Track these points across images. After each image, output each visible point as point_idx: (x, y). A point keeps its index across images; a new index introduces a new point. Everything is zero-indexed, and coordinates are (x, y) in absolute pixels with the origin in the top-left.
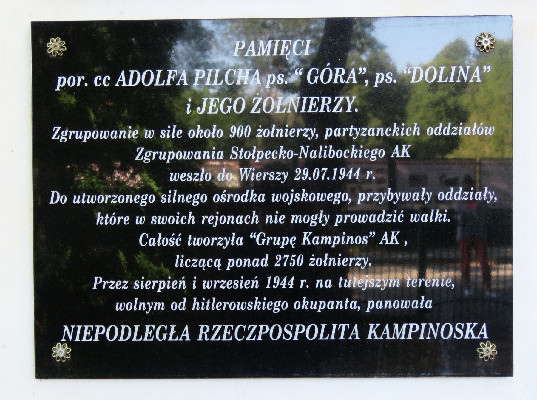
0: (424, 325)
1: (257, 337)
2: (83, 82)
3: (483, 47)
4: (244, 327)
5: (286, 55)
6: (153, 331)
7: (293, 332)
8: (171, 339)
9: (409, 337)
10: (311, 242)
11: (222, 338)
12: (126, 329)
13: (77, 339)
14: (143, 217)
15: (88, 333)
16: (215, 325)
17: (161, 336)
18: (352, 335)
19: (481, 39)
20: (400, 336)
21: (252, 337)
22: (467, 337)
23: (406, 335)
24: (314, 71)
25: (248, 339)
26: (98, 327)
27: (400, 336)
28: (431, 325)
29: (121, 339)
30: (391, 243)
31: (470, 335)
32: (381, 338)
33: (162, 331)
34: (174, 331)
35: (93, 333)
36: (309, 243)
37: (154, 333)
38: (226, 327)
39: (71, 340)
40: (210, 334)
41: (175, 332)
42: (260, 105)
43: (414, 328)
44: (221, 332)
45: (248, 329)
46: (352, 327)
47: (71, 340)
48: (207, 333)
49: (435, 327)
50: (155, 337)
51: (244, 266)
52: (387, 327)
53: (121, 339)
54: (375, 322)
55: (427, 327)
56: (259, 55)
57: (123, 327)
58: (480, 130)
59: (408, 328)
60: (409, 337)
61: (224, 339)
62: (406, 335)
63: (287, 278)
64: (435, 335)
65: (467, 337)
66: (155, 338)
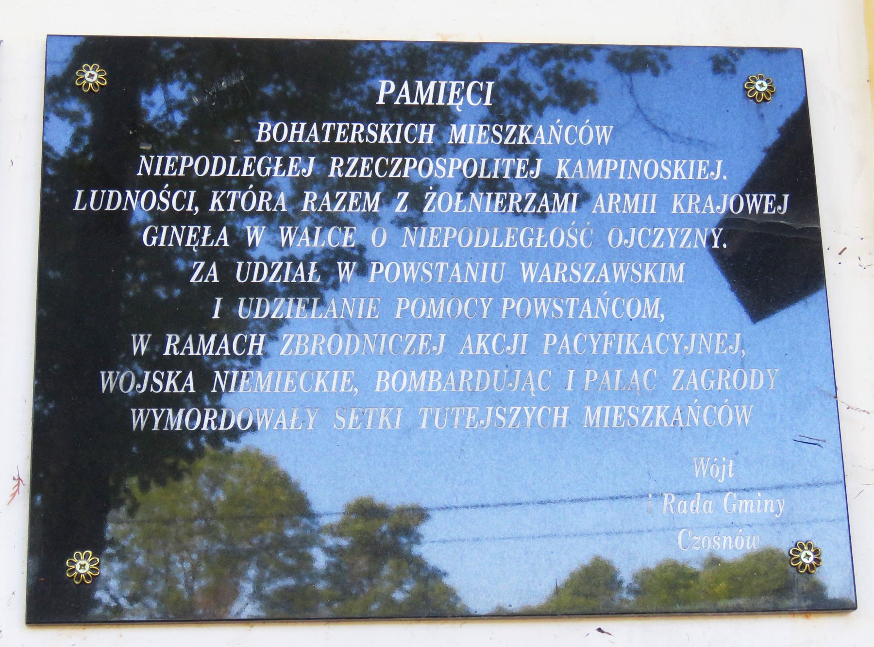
0: (623, 162)
3: (803, 565)
4: (387, 160)
5: (194, 246)
6: (253, 163)
7: (447, 167)
8: (538, 245)
9: (607, 177)
11: (359, 173)
12: (220, 161)
13: (157, 173)
17: (526, 241)
19: (802, 547)
20: (426, 100)
21: (396, 174)
22: (167, 390)
23: (603, 173)
25: (391, 175)
26: (184, 158)
27: (426, 100)
29: (213, 174)
31: (172, 387)
32: (182, 354)
33: (527, 235)
34: (280, 164)
35: (178, 165)
37: (255, 166)
38: (365, 160)
39: (149, 174)
40: (345, 168)
41: (282, 165)
43: (612, 164)
44: (358, 167)
45: (392, 163)
47: (149, 174)
48: (340, 167)
49: (637, 164)
50: (256, 172)
53: (213, 174)
55: (628, 164)
57: (216, 158)
59: (605, 163)
60: (607, 177)
61: (362, 175)
62: (603, 173)
65: (167, 390)
66: (256, 173)
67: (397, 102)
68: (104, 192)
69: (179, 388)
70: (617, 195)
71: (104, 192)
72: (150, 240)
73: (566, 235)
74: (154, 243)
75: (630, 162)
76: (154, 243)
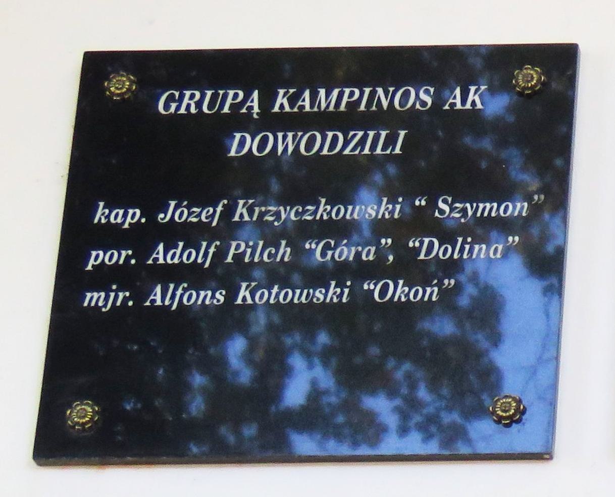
0: (367, 91)
1: (362, 149)
2: (128, 258)
10: (253, 298)
14: (513, 238)
15: (190, 102)
16: (352, 131)
18: (300, 106)
21: (353, 149)
24: (328, 244)
28: (380, 91)
29: (325, 152)
30: (468, 106)
32: (296, 110)
36: (249, 301)
42: (346, 143)
43: (352, 94)
46: (247, 96)
49: (386, 93)
51: (426, 299)
52: (307, 94)
53: (325, 152)
54: (287, 86)
55: (373, 94)
56: (316, 109)
58: (191, 298)
63: (171, 307)
64: (385, 104)
67: (244, 111)
68: (221, 92)
69: (292, 107)
70: (163, 112)
71: (221, 92)
72: (167, 106)
73: (417, 95)
74: (172, 110)
75: (376, 92)
76: (172, 110)
